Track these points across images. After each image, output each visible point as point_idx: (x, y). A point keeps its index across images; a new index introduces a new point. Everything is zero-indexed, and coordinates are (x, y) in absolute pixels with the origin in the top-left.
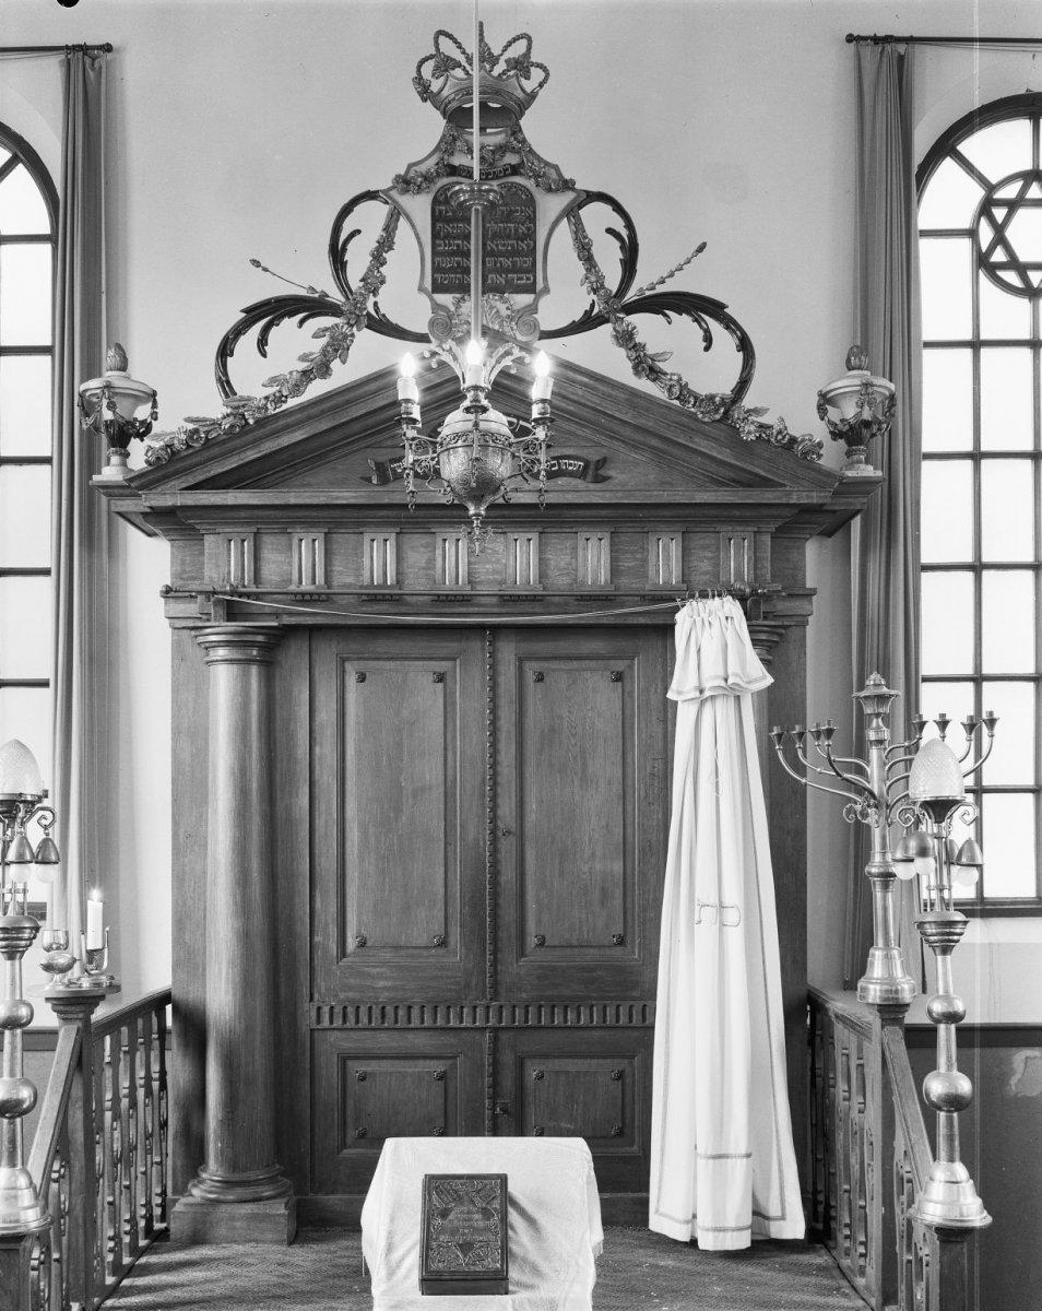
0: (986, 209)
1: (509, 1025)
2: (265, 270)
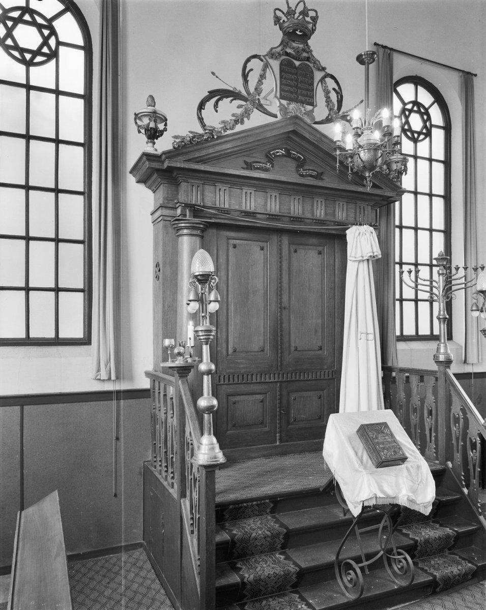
1: (295, 379)
2: (217, 77)
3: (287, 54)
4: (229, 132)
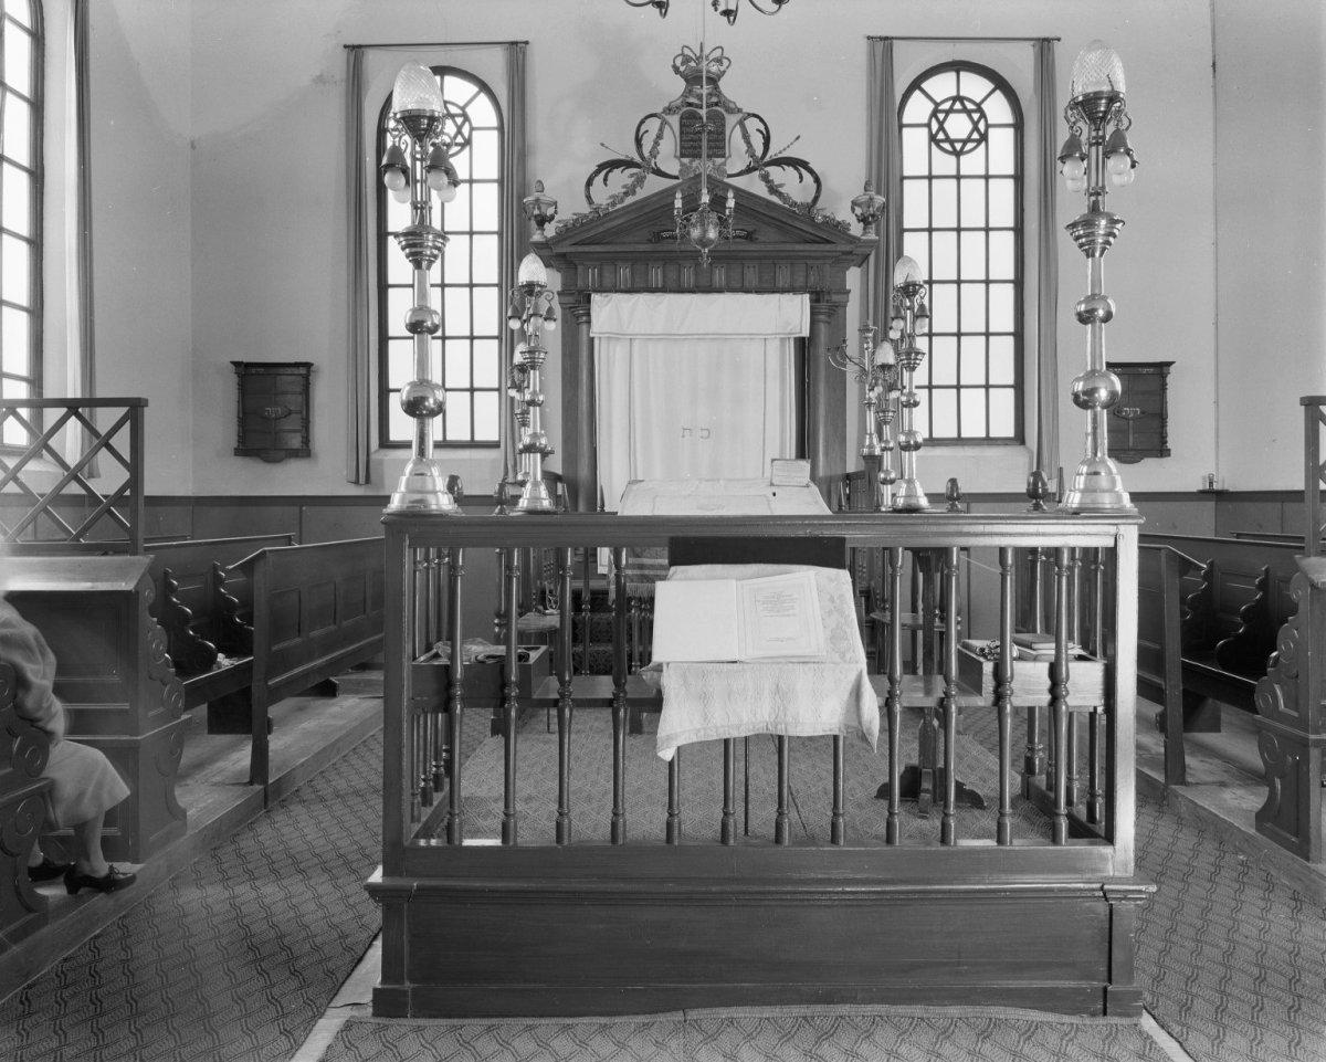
3: (690, 105)
4: (619, 206)
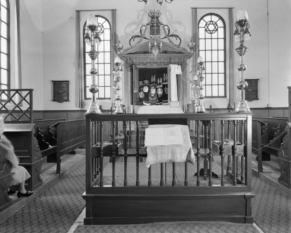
0: (206, 25)
3: (152, 23)
